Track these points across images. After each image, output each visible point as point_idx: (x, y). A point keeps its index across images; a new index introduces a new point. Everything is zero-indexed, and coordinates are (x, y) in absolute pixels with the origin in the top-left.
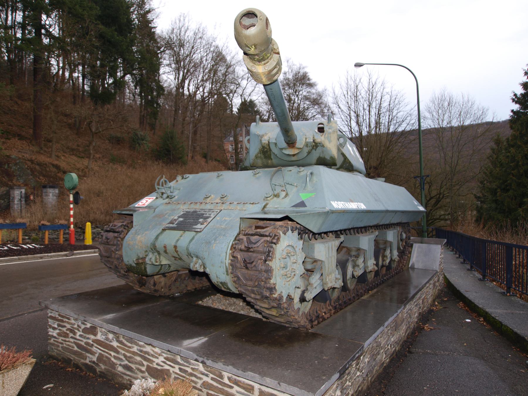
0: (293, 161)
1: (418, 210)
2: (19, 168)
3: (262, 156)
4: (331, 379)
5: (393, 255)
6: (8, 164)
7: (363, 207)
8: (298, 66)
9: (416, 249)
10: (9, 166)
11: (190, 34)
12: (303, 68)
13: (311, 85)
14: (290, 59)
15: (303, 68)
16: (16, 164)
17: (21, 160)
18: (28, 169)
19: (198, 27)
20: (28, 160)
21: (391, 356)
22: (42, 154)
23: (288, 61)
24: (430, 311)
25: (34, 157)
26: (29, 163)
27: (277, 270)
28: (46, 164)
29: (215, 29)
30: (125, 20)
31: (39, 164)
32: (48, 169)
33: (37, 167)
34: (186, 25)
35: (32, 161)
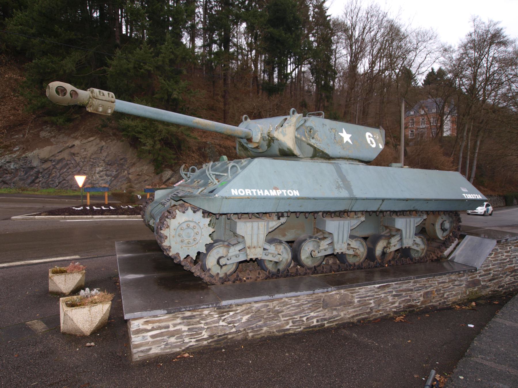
0: (260, 153)
1: (463, 198)
2: (211, 151)
3: (242, 149)
4: (152, 311)
5: (403, 244)
6: (205, 148)
7: (296, 193)
8: (487, 23)
9: (466, 242)
10: (205, 150)
11: (362, 14)
12: (495, 25)
13: (504, 43)
14: (478, 16)
15: (495, 25)
16: (209, 148)
17: (213, 145)
18: (217, 152)
19: (370, 5)
20: (218, 145)
21: (307, 328)
22: (229, 139)
23: (474, 21)
24: (450, 308)
25: (222, 142)
26: (218, 147)
27: (171, 237)
28: (230, 147)
29: (386, 3)
30: (292, 18)
31: (225, 148)
32: (231, 151)
33: (224, 150)
34: (358, 6)
35: (220, 145)
